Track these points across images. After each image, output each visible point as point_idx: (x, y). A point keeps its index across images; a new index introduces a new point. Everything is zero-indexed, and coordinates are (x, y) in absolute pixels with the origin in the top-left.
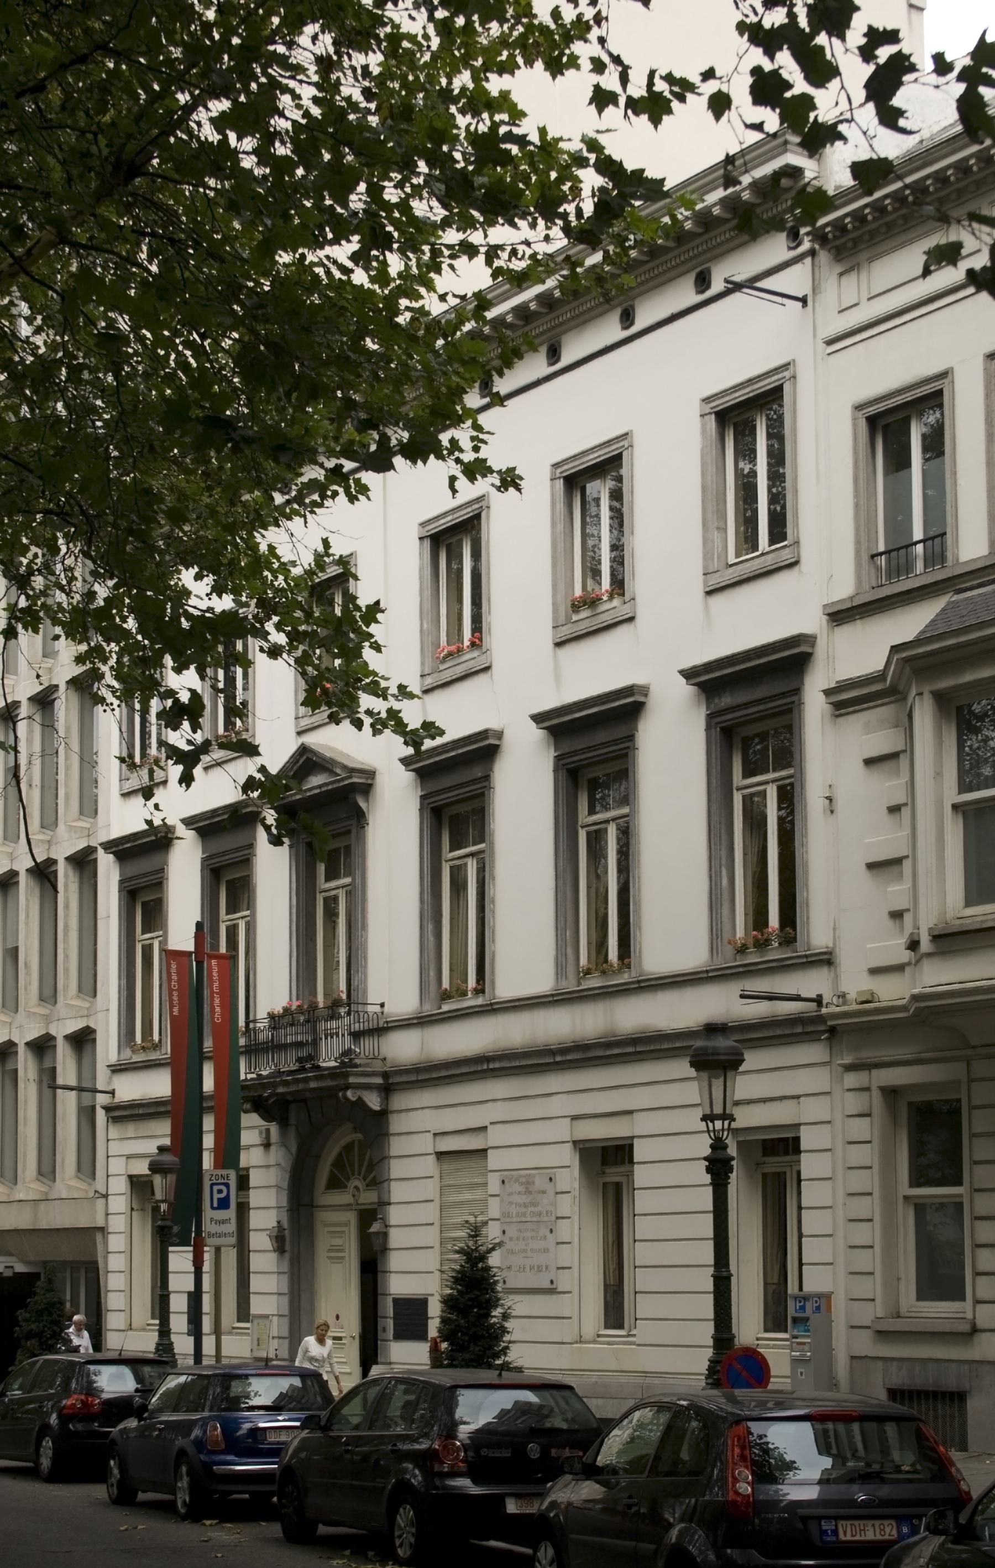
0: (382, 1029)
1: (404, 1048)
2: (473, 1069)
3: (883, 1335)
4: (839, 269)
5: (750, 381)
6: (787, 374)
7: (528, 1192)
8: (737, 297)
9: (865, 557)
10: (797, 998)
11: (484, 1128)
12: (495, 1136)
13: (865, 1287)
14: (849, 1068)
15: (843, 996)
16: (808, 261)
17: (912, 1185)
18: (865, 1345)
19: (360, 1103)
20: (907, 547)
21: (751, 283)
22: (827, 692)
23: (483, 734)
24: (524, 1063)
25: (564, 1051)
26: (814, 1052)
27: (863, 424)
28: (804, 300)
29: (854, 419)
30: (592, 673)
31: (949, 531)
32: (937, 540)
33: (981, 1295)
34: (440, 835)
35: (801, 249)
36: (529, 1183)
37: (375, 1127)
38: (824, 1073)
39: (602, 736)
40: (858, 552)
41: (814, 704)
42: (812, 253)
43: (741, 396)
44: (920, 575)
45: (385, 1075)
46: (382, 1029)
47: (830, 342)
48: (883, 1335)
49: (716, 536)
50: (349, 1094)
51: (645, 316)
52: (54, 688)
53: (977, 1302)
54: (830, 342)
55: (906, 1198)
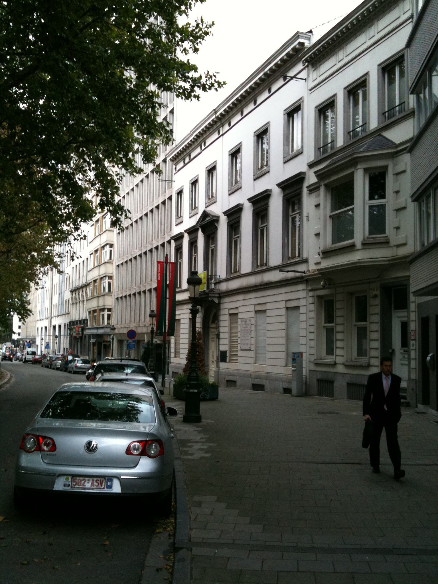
0: (220, 282)
1: (224, 287)
2: (286, 283)
3: (317, 364)
4: (313, 69)
5: (294, 104)
6: (301, 101)
7: (246, 324)
8: (292, 81)
9: (317, 149)
10: (297, 272)
11: (238, 308)
12: (268, 306)
13: (313, 351)
14: (310, 290)
15: (309, 271)
16: (307, 68)
17: (325, 323)
18: (313, 367)
19: (213, 301)
20: (393, 108)
21: (294, 77)
22: (307, 187)
23: (238, 205)
24: (244, 290)
25: (252, 287)
26: (302, 287)
27: (317, 111)
28: (305, 80)
29: (315, 111)
30: (261, 186)
31: (367, 122)
32: (365, 124)
33: (337, 354)
34: (258, 222)
35: (287, 80)
36: (246, 322)
37: (217, 307)
38: (305, 292)
39: (295, 188)
40: (315, 148)
41: (305, 191)
42: (307, 66)
43: (292, 108)
44: (330, 152)
45: (219, 294)
46: (220, 282)
47: (310, 90)
48: (317, 364)
49: (286, 147)
50: (210, 299)
51: (245, 112)
52: (165, 200)
53: (336, 356)
54: (310, 90)
55: (324, 327)
